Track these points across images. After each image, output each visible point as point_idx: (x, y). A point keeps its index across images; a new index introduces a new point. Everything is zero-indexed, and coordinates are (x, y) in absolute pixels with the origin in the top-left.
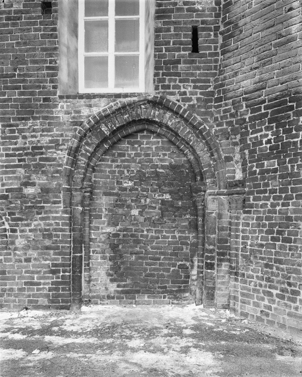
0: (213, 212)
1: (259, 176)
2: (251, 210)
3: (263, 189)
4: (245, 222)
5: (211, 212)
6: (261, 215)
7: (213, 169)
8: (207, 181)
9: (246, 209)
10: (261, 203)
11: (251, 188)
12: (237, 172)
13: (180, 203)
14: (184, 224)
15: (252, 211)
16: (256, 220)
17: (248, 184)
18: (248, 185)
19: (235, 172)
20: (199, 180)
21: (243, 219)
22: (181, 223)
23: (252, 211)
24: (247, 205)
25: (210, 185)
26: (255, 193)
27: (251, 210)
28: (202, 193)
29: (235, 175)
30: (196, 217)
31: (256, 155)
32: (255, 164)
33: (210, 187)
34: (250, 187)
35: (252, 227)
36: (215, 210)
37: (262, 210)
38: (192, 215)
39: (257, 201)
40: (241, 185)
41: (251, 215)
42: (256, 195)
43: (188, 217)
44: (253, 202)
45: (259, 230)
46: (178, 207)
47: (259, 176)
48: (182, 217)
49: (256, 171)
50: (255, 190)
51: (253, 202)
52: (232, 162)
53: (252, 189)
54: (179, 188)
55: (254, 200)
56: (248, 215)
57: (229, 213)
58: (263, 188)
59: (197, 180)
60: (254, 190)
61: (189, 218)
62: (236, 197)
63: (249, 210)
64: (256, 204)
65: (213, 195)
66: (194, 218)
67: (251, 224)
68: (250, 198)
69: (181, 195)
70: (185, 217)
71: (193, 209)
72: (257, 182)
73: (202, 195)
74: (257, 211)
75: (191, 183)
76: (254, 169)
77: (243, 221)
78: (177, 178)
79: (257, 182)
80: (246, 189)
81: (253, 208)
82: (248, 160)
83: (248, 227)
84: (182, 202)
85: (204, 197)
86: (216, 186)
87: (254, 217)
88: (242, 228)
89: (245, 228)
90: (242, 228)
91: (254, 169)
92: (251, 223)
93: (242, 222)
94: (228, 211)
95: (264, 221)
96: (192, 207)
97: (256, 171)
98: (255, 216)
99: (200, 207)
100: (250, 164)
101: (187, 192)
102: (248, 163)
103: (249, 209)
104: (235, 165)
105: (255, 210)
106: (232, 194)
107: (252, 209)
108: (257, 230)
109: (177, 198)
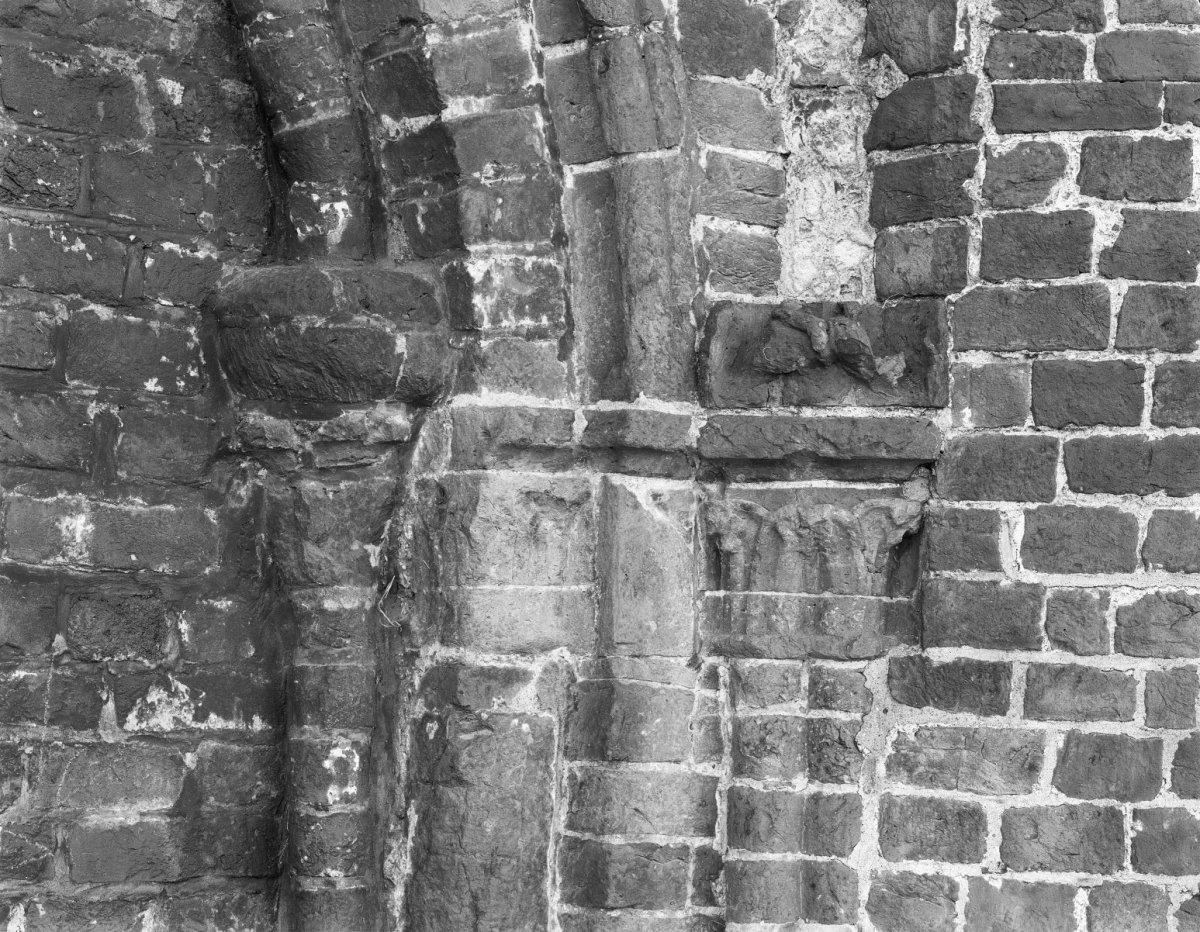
0: (521, 663)
1: (1118, 290)
2: (1000, 671)
3: (1155, 434)
4: (919, 803)
5: (503, 663)
6: (1135, 728)
7: (540, 123)
8: (476, 270)
9: (941, 655)
10: (1126, 590)
11: (1013, 419)
12: (795, 215)
13: (79, 526)
14: (122, 814)
15: (1019, 673)
16: (1066, 782)
17: (977, 359)
18: (975, 376)
19: (782, 209)
20: (335, 236)
21: (902, 763)
22: (85, 796)
23: (1019, 673)
24: (951, 602)
25: (509, 323)
26: (1061, 478)
27: (1000, 671)
28: (382, 410)
29: (784, 235)
30: (258, 724)
31: (1088, 40)
32: (1070, 142)
33: (503, 344)
34: (988, 390)
35: (1010, 858)
36: (545, 648)
37: (1140, 668)
38: (212, 694)
39: (1078, 568)
40: (892, 366)
41: (995, 721)
42: (1064, 496)
43: (164, 721)
44: (1031, 577)
45: (1097, 896)
46: (46, 578)
47: (1118, 290)
48: (89, 719)
49: (1077, 226)
50: (1064, 437)
51: (1031, 577)
52: (755, 77)
53: (1025, 430)
54: (63, 315)
55: (1042, 548)
56: (967, 719)
57: (701, 692)
58: (1159, 422)
59: (318, 242)
60: (1053, 444)
61: (185, 739)
62: (821, 498)
63: (981, 667)
64: (1066, 601)
65: (546, 454)
66: (240, 737)
67: (994, 825)
68: (991, 521)
69: (93, 410)
70: (132, 722)
71: (231, 618)
72: (1091, 357)
73: (383, 445)
74: (1080, 678)
75: (210, 267)
76: (1064, 196)
77: (902, 789)
78: (51, 169)
79: (1091, 357)
80: (943, 419)
81: (1028, 642)
82: (983, 86)
83: (960, 857)
84: (97, 516)
85: (400, 467)
86: (564, 353)
87: (1037, 743)
88: (882, 865)
89: (924, 867)
90: (882, 865)
91: (1064, 196)
92: (993, 809)
93: (888, 805)
94: (694, 663)
95: (1166, 799)
96: (215, 588)
97: (1077, 226)
98: (1054, 735)
99: (347, 599)
100: (1013, 141)
101: (166, 380)
102: (982, 112)
103: (968, 653)
104: (786, 125)
105: (1059, 673)
106: (765, 467)
107: (1019, 660)
108: (1082, 899)
109: (46, 450)
